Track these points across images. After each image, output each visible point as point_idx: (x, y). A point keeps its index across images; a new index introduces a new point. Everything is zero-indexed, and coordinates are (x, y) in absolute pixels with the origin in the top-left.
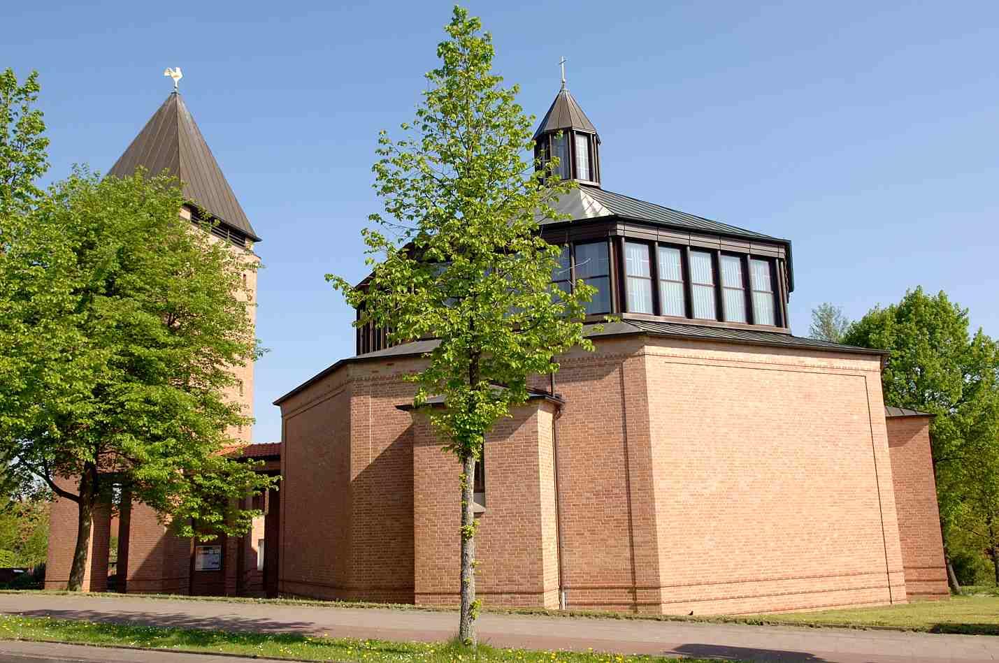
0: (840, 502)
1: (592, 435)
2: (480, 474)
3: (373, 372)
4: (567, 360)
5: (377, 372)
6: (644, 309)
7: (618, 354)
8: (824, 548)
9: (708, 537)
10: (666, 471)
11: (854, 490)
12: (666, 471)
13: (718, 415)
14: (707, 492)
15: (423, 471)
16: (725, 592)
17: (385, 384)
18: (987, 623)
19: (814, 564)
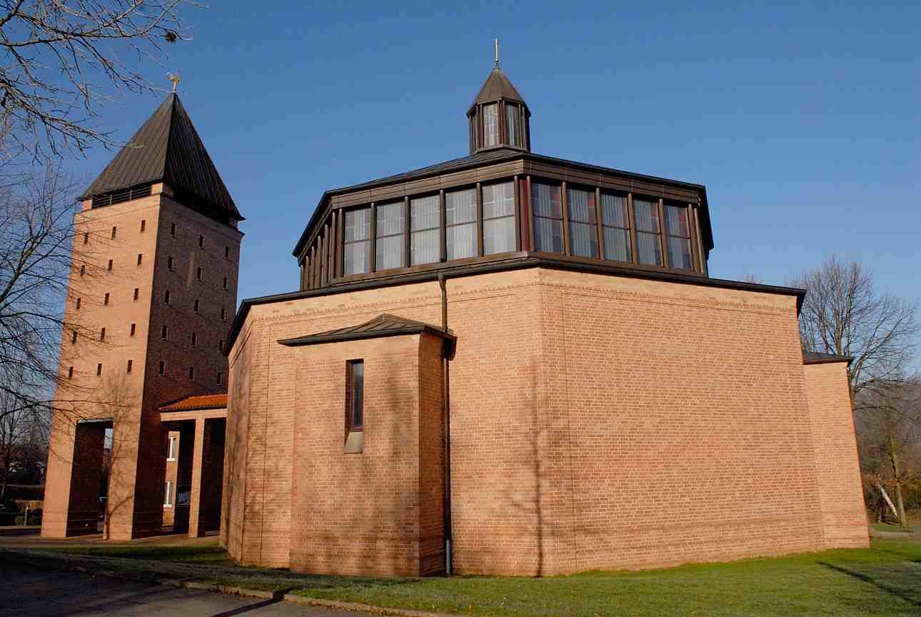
0: (755, 446)
1: (483, 371)
2: (446, 412)
3: (274, 311)
4: (459, 293)
5: (278, 311)
6: (541, 222)
7: (510, 284)
8: (737, 494)
9: (608, 481)
10: (561, 409)
11: (769, 432)
12: (561, 409)
13: (467, 513)
14: (608, 433)
15: (304, 408)
16: (627, 541)
17: (285, 323)
18: (845, 547)
19: (727, 512)
